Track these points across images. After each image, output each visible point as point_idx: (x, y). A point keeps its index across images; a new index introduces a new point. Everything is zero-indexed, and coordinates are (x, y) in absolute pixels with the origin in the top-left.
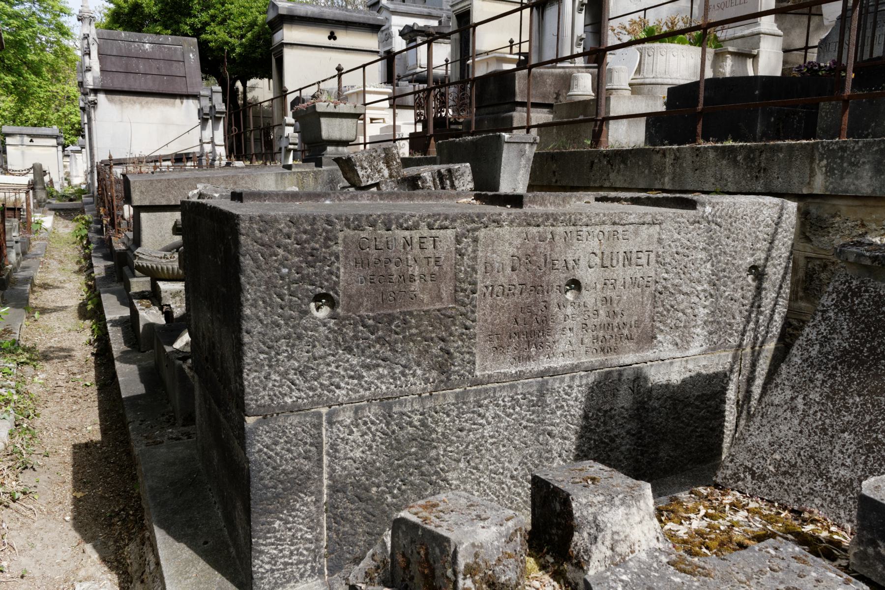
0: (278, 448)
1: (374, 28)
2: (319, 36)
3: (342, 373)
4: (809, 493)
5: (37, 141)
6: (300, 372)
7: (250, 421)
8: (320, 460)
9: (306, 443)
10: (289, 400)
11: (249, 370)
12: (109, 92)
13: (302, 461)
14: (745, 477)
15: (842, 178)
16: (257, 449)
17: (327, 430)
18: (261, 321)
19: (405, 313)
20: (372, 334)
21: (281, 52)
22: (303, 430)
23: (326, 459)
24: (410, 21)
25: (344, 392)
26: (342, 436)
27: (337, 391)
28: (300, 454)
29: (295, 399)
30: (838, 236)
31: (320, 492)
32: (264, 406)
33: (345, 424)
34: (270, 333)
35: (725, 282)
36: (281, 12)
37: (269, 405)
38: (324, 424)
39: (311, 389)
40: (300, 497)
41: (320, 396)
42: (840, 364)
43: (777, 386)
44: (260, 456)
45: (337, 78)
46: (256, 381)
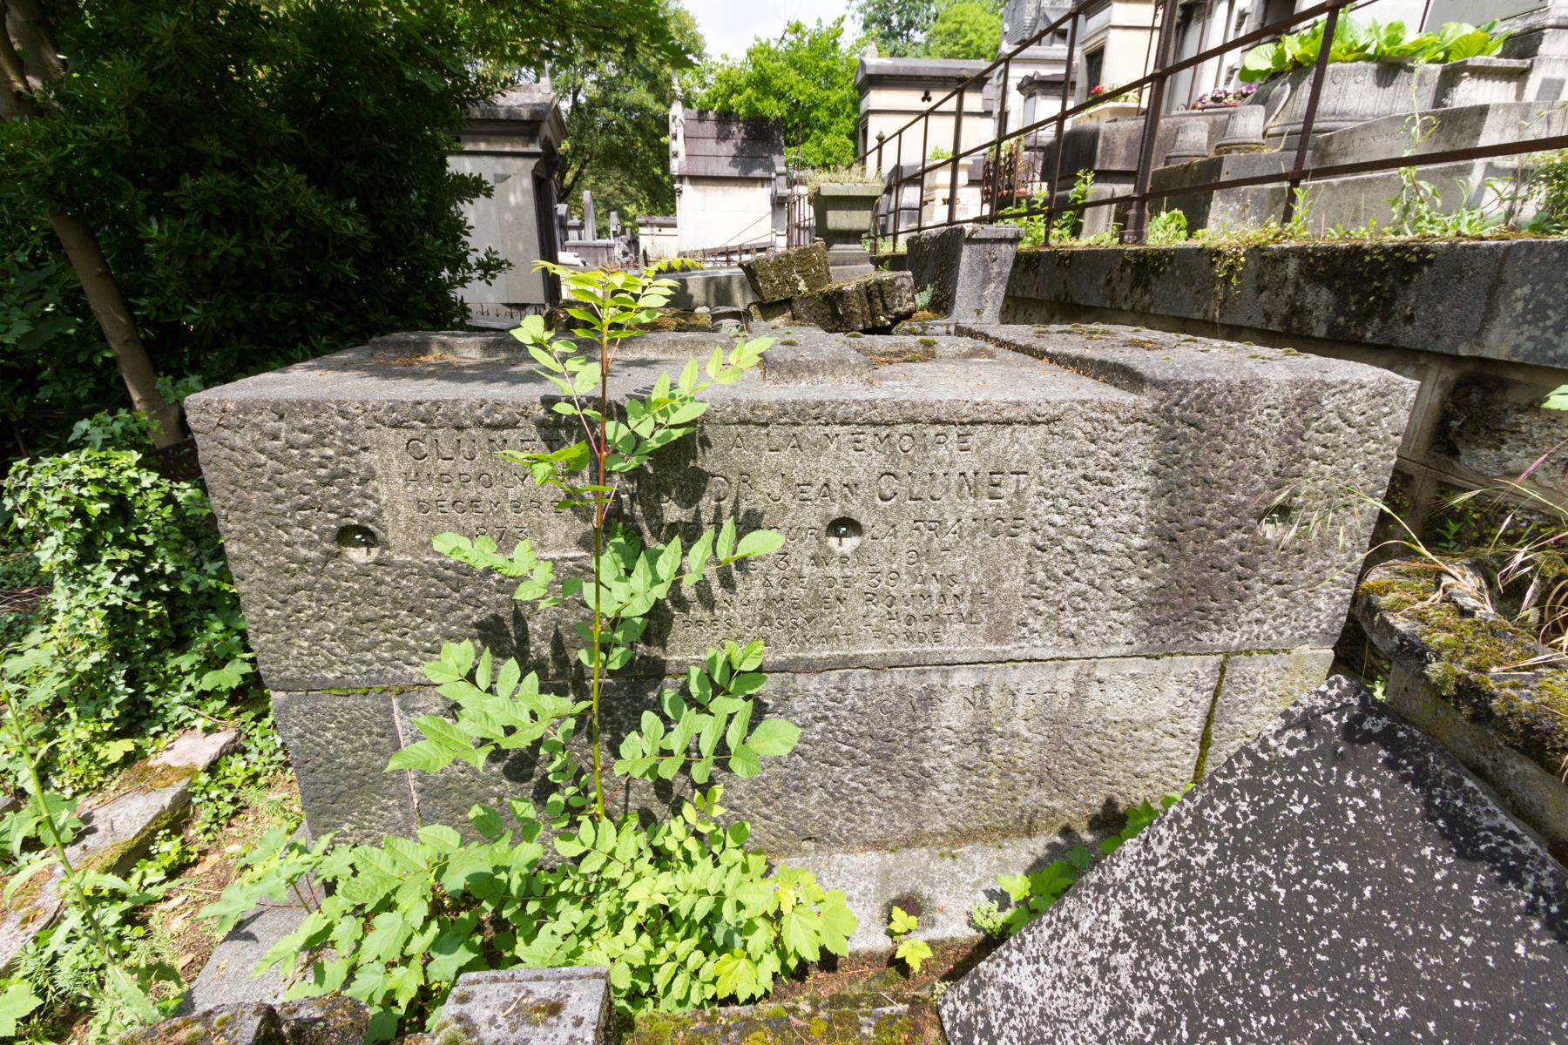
0: (329, 735)
3: (413, 643)
10: (331, 676)
12: (696, 179)
24: (1029, 71)
27: (409, 668)
28: (364, 746)
30: (1521, 453)
35: (1198, 534)
36: (870, 71)
41: (379, 672)
45: (962, 150)
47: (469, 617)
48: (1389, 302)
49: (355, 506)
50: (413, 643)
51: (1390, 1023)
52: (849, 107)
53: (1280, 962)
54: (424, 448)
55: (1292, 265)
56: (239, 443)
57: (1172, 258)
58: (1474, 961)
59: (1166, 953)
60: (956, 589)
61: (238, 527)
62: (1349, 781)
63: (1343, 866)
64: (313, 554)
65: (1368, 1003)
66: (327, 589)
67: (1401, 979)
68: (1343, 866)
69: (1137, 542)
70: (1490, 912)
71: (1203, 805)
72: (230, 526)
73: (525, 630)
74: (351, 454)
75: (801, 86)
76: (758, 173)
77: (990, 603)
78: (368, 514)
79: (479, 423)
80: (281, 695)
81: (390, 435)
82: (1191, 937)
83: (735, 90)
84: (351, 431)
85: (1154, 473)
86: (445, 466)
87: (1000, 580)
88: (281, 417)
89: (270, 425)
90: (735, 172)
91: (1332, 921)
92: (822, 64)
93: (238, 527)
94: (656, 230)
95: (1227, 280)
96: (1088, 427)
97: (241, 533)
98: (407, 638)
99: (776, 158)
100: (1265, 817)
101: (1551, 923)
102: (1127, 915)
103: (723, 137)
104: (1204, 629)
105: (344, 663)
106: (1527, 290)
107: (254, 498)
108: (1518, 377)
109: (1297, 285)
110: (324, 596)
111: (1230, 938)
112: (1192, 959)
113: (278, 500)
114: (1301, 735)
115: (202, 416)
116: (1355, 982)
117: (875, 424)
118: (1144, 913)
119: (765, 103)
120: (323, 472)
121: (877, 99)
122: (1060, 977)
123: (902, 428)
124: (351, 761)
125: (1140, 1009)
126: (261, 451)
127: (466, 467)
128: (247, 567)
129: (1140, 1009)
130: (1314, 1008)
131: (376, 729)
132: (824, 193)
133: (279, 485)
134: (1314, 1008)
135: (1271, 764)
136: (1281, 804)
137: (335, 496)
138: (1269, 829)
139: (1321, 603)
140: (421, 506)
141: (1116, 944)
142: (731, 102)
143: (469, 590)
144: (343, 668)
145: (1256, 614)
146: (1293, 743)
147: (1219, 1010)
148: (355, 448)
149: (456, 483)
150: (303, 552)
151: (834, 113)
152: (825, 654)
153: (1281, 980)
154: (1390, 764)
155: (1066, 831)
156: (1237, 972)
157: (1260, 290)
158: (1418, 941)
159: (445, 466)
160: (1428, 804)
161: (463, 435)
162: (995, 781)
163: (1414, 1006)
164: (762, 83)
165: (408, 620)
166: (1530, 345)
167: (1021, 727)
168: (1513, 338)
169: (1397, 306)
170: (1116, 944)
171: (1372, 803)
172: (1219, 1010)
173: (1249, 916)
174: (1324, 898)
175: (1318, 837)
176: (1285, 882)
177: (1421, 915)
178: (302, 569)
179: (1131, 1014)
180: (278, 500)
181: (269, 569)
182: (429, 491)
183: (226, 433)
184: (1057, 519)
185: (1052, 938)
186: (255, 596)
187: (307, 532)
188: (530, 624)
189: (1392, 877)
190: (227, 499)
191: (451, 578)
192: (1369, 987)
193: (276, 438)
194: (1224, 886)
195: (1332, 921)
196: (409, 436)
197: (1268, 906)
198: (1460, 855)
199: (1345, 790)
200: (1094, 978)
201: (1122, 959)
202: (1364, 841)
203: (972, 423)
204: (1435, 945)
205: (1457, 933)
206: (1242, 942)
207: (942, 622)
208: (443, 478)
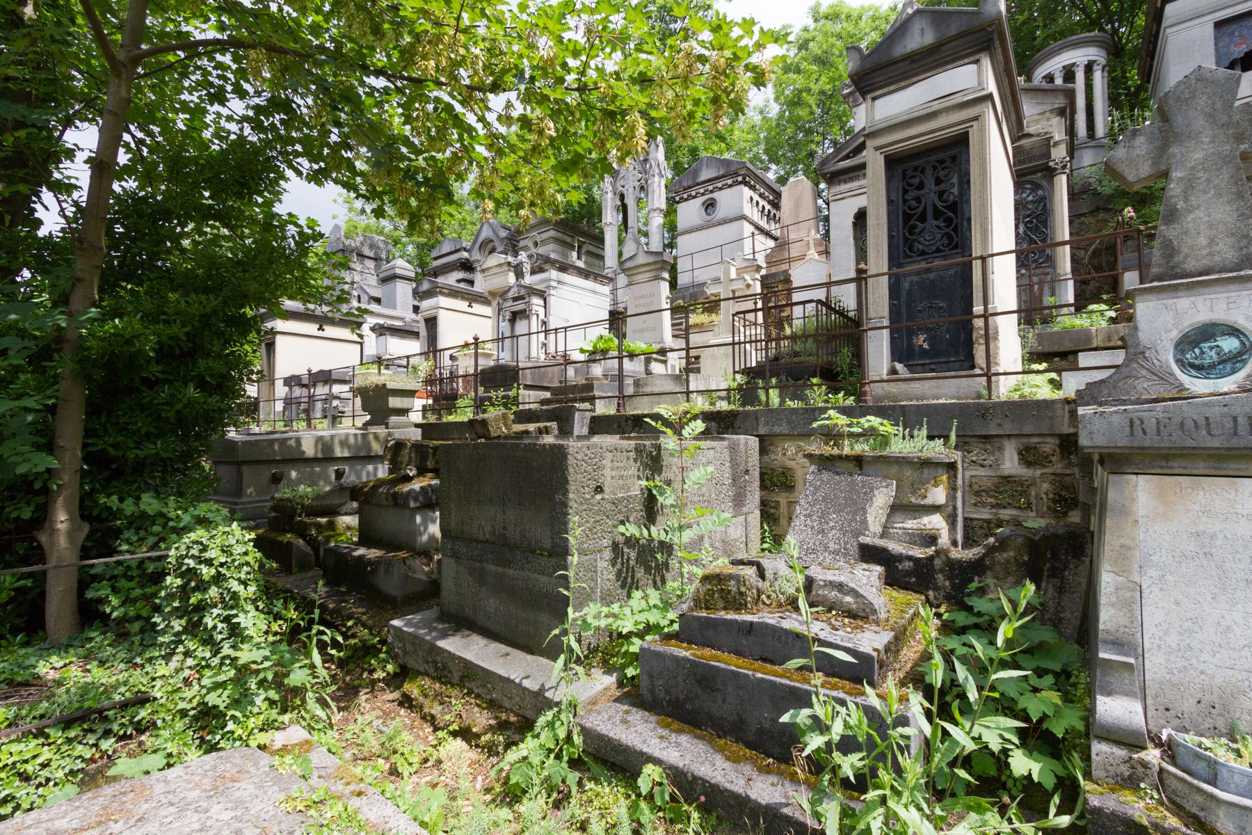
132: (388, 387)
182: (614, 473)
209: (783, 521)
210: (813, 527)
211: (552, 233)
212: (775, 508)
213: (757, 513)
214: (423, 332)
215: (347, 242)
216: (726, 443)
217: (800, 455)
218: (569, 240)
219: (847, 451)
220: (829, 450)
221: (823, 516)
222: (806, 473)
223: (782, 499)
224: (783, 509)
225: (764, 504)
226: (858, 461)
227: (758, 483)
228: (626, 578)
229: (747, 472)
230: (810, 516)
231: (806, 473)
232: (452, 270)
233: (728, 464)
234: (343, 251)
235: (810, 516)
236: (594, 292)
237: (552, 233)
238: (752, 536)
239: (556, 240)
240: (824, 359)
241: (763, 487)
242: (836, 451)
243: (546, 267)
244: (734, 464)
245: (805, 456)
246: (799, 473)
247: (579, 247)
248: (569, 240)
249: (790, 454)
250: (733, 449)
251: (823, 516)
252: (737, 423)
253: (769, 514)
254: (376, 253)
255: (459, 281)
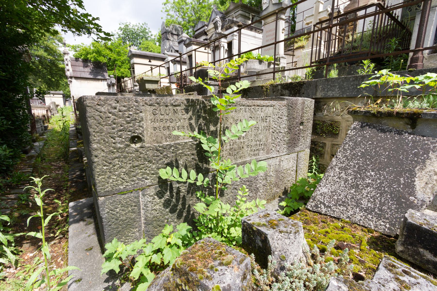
0: (118, 210)
1: (163, 59)
2: (146, 61)
3: (148, 172)
4: (353, 214)
5: (55, 96)
6: (127, 174)
7: (101, 199)
8: (140, 212)
9: (132, 206)
10: (122, 187)
11: (99, 175)
12: (77, 78)
13: (131, 214)
14: (321, 206)
15: (327, 92)
16: (106, 211)
17: (142, 199)
18: (103, 151)
19: (175, 144)
20: (161, 154)
21: (134, 66)
22: (130, 200)
23: (142, 212)
25: (149, 181)
26: (149, 200)
27: (146, 181)
28: (129, 211)
29: (125, 186)
31: (141, 226)
32: (108, 191)
33: (151, 195)
34: (109, 156)
36: (133, 53)
37: (111, 191)
38: (141, 196)
39: (133, 181)
40: (130, 230)
41: (137, 184)
42: (361, 158)
43: (332, 168)
44: (108, 215)
46: (103, 180)
47: (164, 161)
48: (299, 91)
49: (137, 129)
50: (148, 172)
51: (386, 155)
52: (127, 62)
53: (368, 158)
54: (157, 112)
55: (279, 87)
56: (103, 109)
57: (252, 88)
58: (392, 143)
59: (350, 169)
60: (261, 143)
61: (98, 138)
62: (365, 132)
63: (370, 142)
64: (122, 146)
65: (383, 155)
66: (125, 157)
67: (385, 149)
68: (370, 142)
69: (286, 130)
70: (391, 137)
71: (344, 147)
72: (95, 138)
73: (178, 164)
74: (137, 114)
75: (111, 55)
76: (99, 77)
77: (266, 146)
78: (140, 132)
79: (172, 105)
80: (103, 198)
81: (148, 108)
82: (352, 164)
83: (88, 54)
84: (138, 106)
85: (287, 116)
86: (162, 117)
87: (268, 140)
88: (118, 102)
89: (114, 105)
90: (92, 77)
91: (372, 149)
92: (116, 50)
93: (98, 138)
94: (52, 95)
95: (266, 91)
96: (279, 107)
97: (99, 140)
98: (147, 171)
99: (105, 74)
100: (355, 143)
101: (398, 134)
102: (339, 168)
103: (85, 66)
104: (295, 147)
105: (127, 182)
106: (321, 86)
107: (105, 128)
108: (322, 100)
109: (281, 90)
110: (124, 160)
111: (359, 160)
112: (355, 166)
113: (113, 129)
114: (354, 131)
115: (92, 101)
116: (380, 154)
117: (248, 106)
118: (342, 166)
119: (100, 58)
120: (128, 119)
121: (136, 60)
122: (332, 185)
123: (253, 107)
124: (124, 218)
125: (349, 179)
126: (110, 113)
127: (167, 117)
128: (99, 152)
129: (349, 179)
130: (376, 160)
131: (134, 204)
132: (144, 79)
133: (114, 124)
134: (376, 160)
135: (352, 136)
136: (356, 140)
137: (131, 127)
138: (357, 144)
139: (308, 140)
140: (155, 129)
141: (340, 173)
142: (88, 57)
143: (165, 153)
144: (126, 184)
145: (301, 144)
146: (354, 132)
147: (363, 169)
148: (139, 112)
149: (164, 122)
150: (119, 145)
151: (123, 63)
152: (240, 161)
153: (370, 160)
154: (369, 128)
155: (280, 197)
156: (362, 163)
157: (274, 92)
158: (384, 144)
159: (162, 117)
160: (377, 130)
161: (167, 108)
162: (268, 188)
163: (388, 151)
164: (98, 52)
165: (148, 165)
166: (324, 95)
167: (271, 173)
168: (321, 94)
169: (301, 91)
170: (340, 173)
171: (370, 133)
172: (363, 169)
173: (360, 156)
174: (370, 147)
175: (364, 141)
176: (363, 149)
177: (383, 142)
178: (117, 151)
179: (349, 180)
180: (113, 129)
181: (106, 152)
182: (157, 125)
183: (99, 107)
184: (275, 126)
185: (326, 181)
186: (100, 163)
187: (121, 139)
188: (179, 162)
189: (377, 140)
190: (96, 129)
191: (161, 150)
192: (382, 153)
193: (115, 108)
194: (354, 154)
195: (372, 149)
196: (153, 108)
197: (362, 153)
198: (384, 133)
199: (365, 134)
200: (339, 180)
201: (343, 174)
202: (371, 138)
203: (263, 106)
204: (387, 144)
205: (388, 141)
206: (361, 159)
207: (259, 151)
208: (162, 120)
209: (327, 156)
210: (346, 181)
211: (240, 12)
212: (322, 147)
213: (308, 151)
214: (188, 61)
215: (167, 29)
216: (285, 102)
217: (346, 112)
218: (247, 15)
219: (398, 107)
220: (373, 108)
221: (360, 172)
222: (350, 128)
223: (328, 142)
224: (328, 148)
225: (313, 142)
226: (413, 120)
227: (310, 131)
228: (176, 206)
229: (302, 123)
230: (345, 169)
231: (350, 128)
232: (202, 36)
233: (285, 118)
234: (166, 32)
235: (345, 169)
236: (255, 37)
237: (240, 12)
238: (301, 166)
239: (242, 15)
240: (375, 49)
241: (315, 131)
242: (385, 108)
243: (232, 25)
244: (290, 117)
245: (350, 113)
246: (343, 125)
247: (252, 19)
248: (247, 15)
249: (336, 110)
250: (291, 107)
251: (360, 172)
252: (303, 90)
253: (316, 150)
254: (178, 33)
255: (204, 40)
